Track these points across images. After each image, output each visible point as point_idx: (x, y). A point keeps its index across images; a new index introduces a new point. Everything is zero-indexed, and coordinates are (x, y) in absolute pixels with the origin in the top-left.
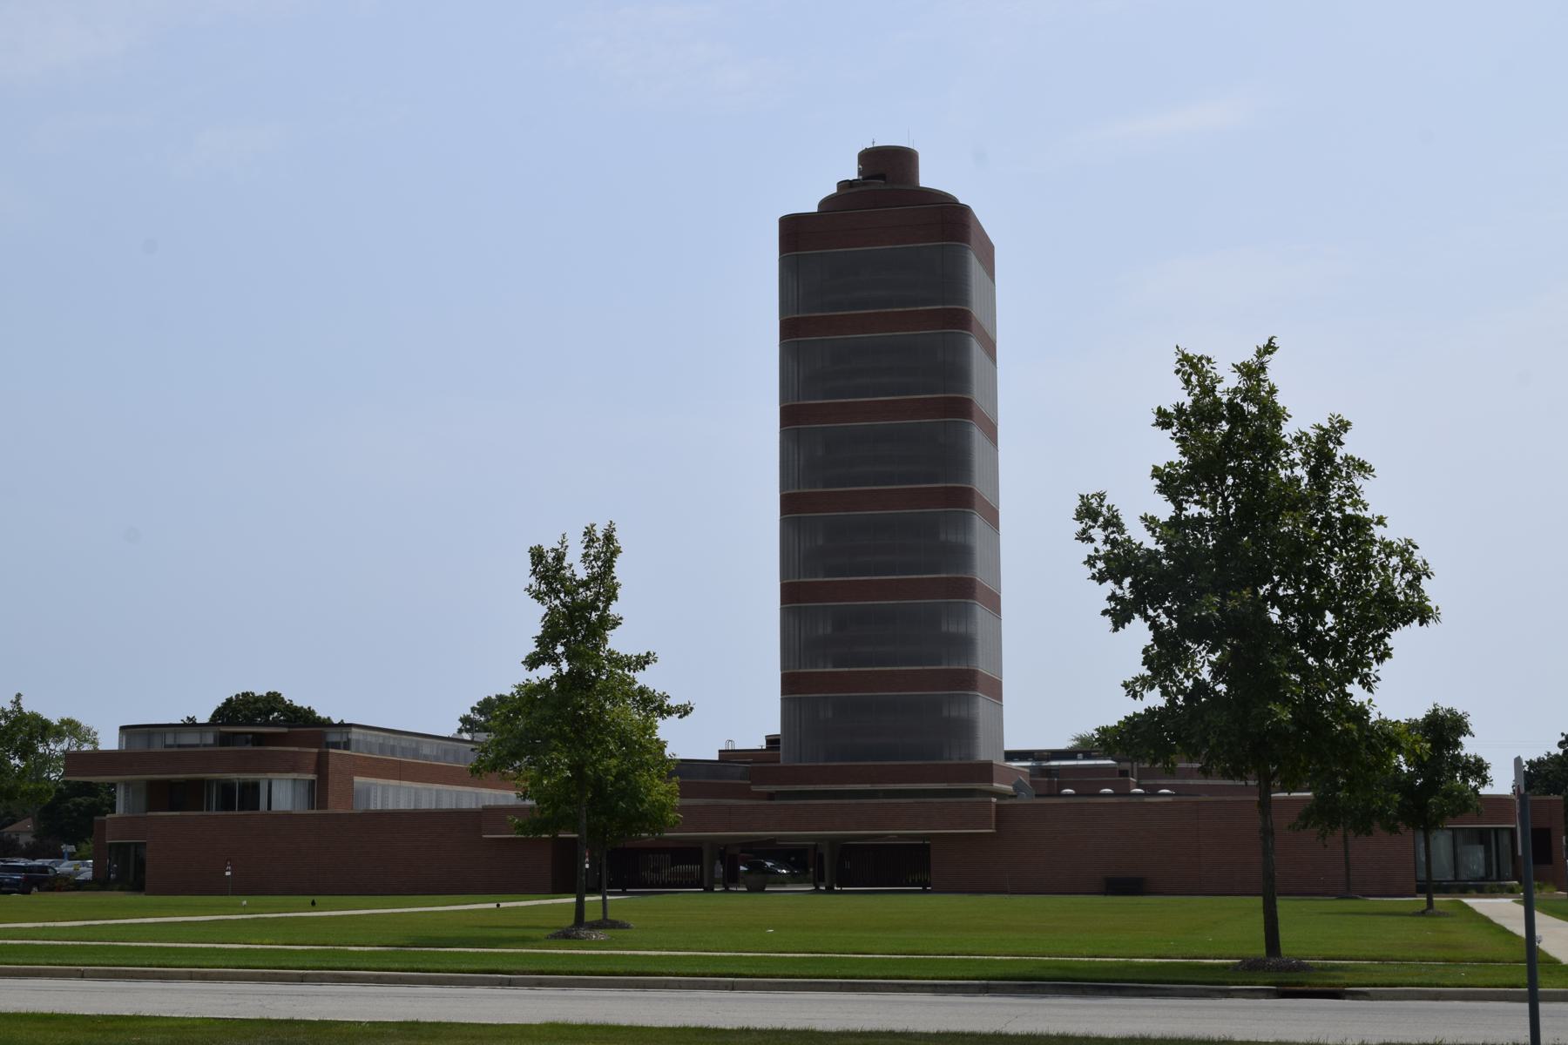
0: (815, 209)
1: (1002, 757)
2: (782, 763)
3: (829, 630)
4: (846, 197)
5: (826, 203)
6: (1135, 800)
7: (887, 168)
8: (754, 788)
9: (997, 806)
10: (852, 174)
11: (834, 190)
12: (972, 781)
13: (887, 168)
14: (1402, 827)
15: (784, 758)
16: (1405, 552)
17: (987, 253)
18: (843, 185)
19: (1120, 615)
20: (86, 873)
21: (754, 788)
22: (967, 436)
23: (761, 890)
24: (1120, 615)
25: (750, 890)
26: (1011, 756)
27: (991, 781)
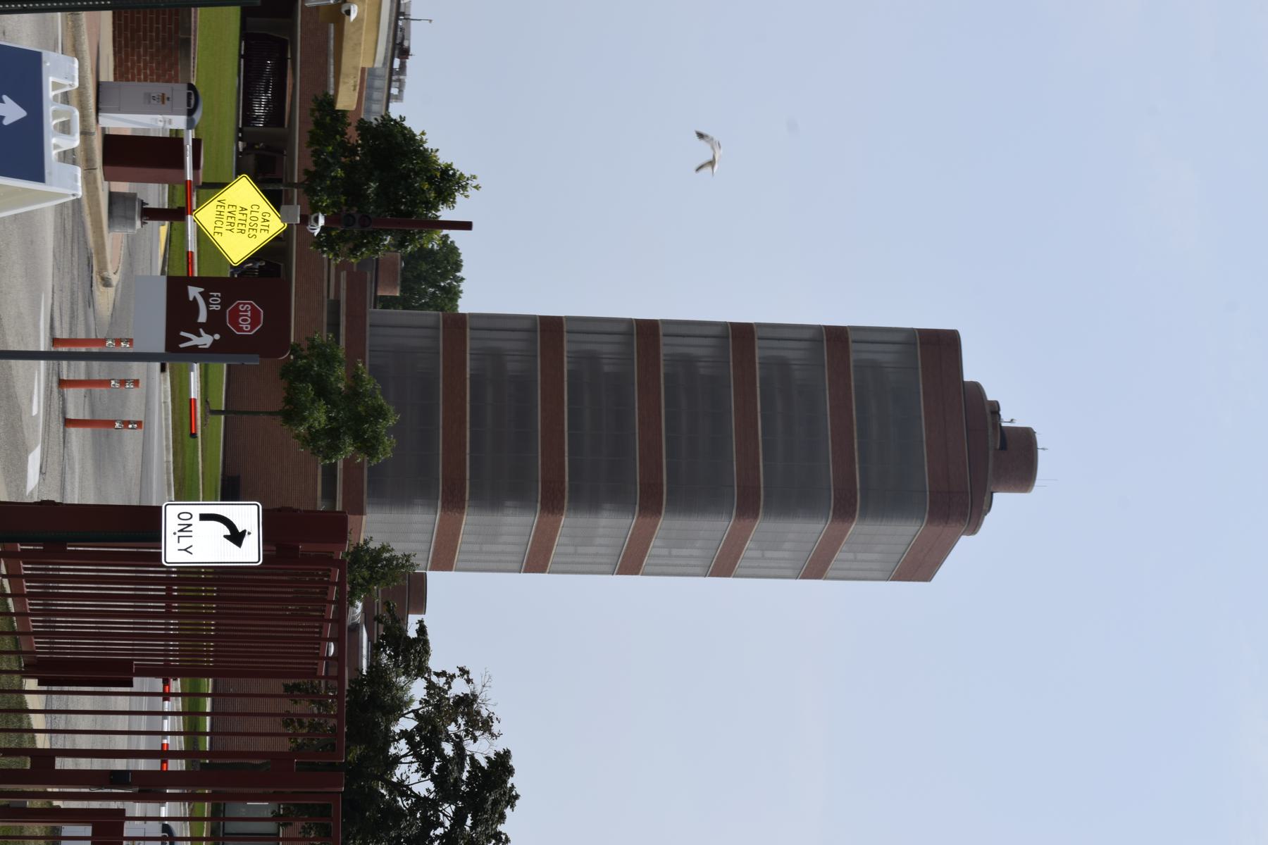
5: (976, 390)
7: (1014, 458)
11: (990, 396)
13: (1014, 458)
17: (919, 566)
18: (995, 408)
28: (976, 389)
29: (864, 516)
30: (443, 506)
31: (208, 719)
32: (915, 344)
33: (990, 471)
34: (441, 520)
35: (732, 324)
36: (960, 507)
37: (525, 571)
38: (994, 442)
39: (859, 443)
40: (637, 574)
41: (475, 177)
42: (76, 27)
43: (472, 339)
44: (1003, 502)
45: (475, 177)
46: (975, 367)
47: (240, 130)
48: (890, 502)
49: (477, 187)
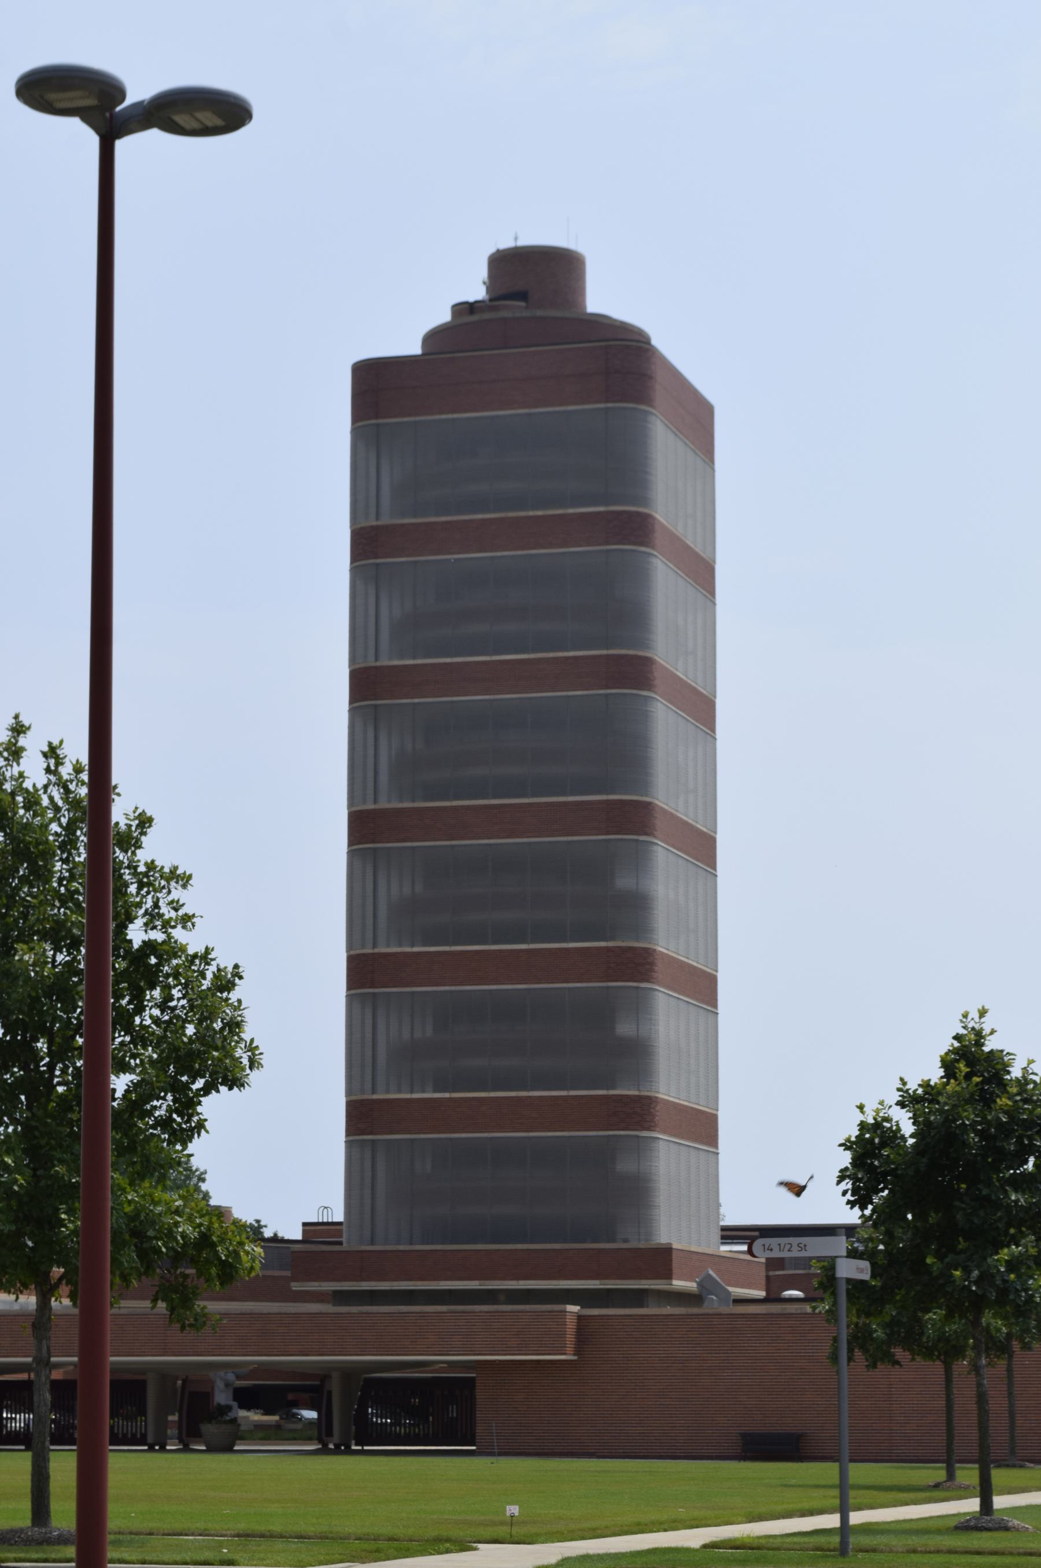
0: (414, 347)
1: (716, 1235)
2: (345, 1247)
3: (429, 1032)
4: (464, 333)
5: (434, 338)
6: (791, 1308)
7: (534, 281)
8: (296, 1286)
9: (580, 1318)
10: (477, 292)
11: (446, 317)
12: (641, 1276)
13: (534, 281)
14: (899, 1353)
15: (348, 1243)
16: (251, 1048)
17: (697, 420)
18: (463, 310)
19: (218, 1091)
20: (204, 1448)
21: (296, 1286)
22: (643, 718)
23: (229, 1449)
24: (218, 1091)
25: (210, 1450)
26: (731, 1234)
27: (668, 1276)
28: (432, 338)
29: (645, 501)
30: (649, 1129)
31: (832, 1521)
32: (378, 425)
33: (558, 314)
34: (664, 1132)
35: (351, 702)
36: (624, 362)
37: (716, 1006)
38: (516, 309)
39: (534, 508)
40: (714, 840)
41: (965, 1016)
42: (832, 1487)
43: (388, 1092)
44: (603, 297)
45: (965, 1016)
46: (402, 335)
47: (151, 1449)
48: (622, 468)
49: (983, 1013)
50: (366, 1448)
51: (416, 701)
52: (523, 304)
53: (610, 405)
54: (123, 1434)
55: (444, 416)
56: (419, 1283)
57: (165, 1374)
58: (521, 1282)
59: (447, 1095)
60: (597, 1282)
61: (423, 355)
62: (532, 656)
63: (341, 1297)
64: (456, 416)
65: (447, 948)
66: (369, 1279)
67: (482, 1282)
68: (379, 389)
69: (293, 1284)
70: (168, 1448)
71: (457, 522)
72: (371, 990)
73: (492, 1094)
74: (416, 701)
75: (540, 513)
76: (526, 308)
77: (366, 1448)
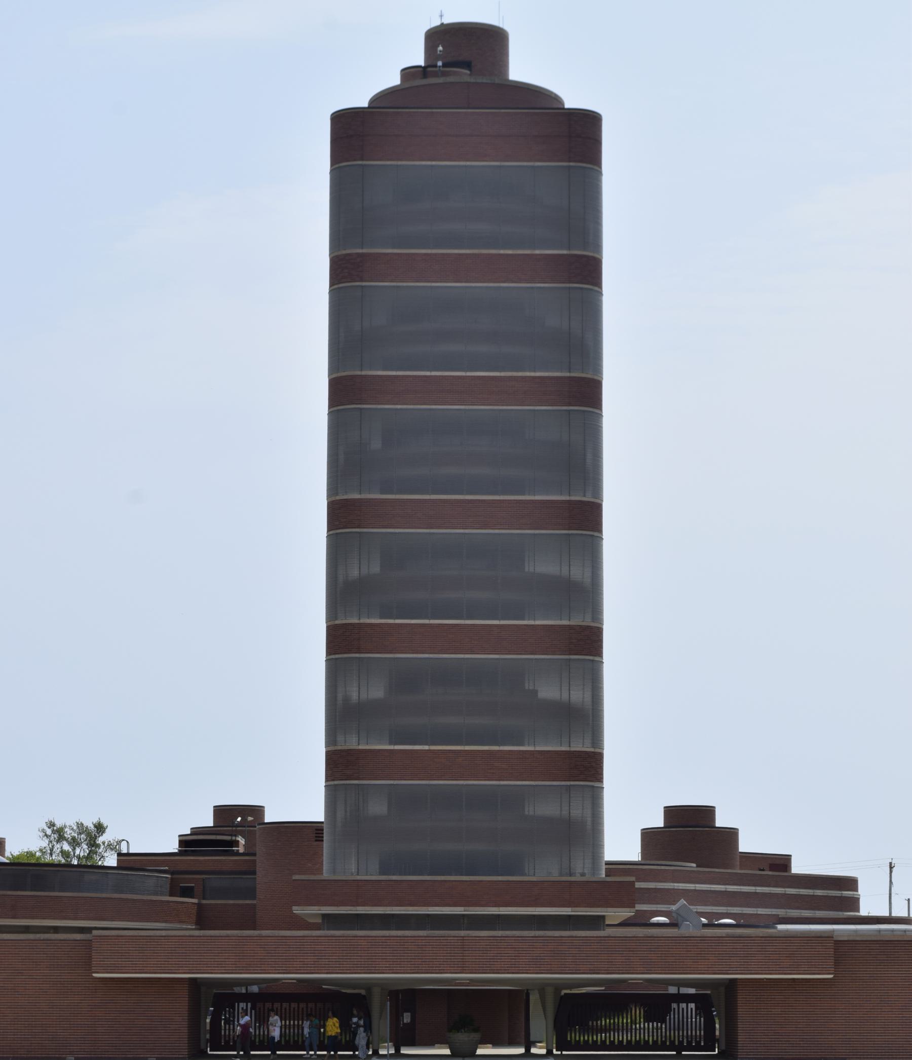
7: (466, 52)
10: (418, 59)
13: (466, 52)
50: (564, 1053)
51: (399, 407)
52: (468, 72)
53: (572, 164)
54: (294, 1041)
55: (424, 163)
56: (411, 908)
57: (542, 987)
58: (501, 909)
59: (426, 747)
60: (569, 909)
61: (369, 107)
62: (503, 374)
63: (330, 921)
64: (434, 163)
65: (426, 621)
66: (364, 904)
67: (467, 908)
68: (352, 132)
69: (294, 908)
70: (381, 1053)
71: (435, 254)
72: (357, 655)
73: (467, 748)
74: (399, 407)
75: (510, 252)
76: (470, 75)
77: (564, 1053)
